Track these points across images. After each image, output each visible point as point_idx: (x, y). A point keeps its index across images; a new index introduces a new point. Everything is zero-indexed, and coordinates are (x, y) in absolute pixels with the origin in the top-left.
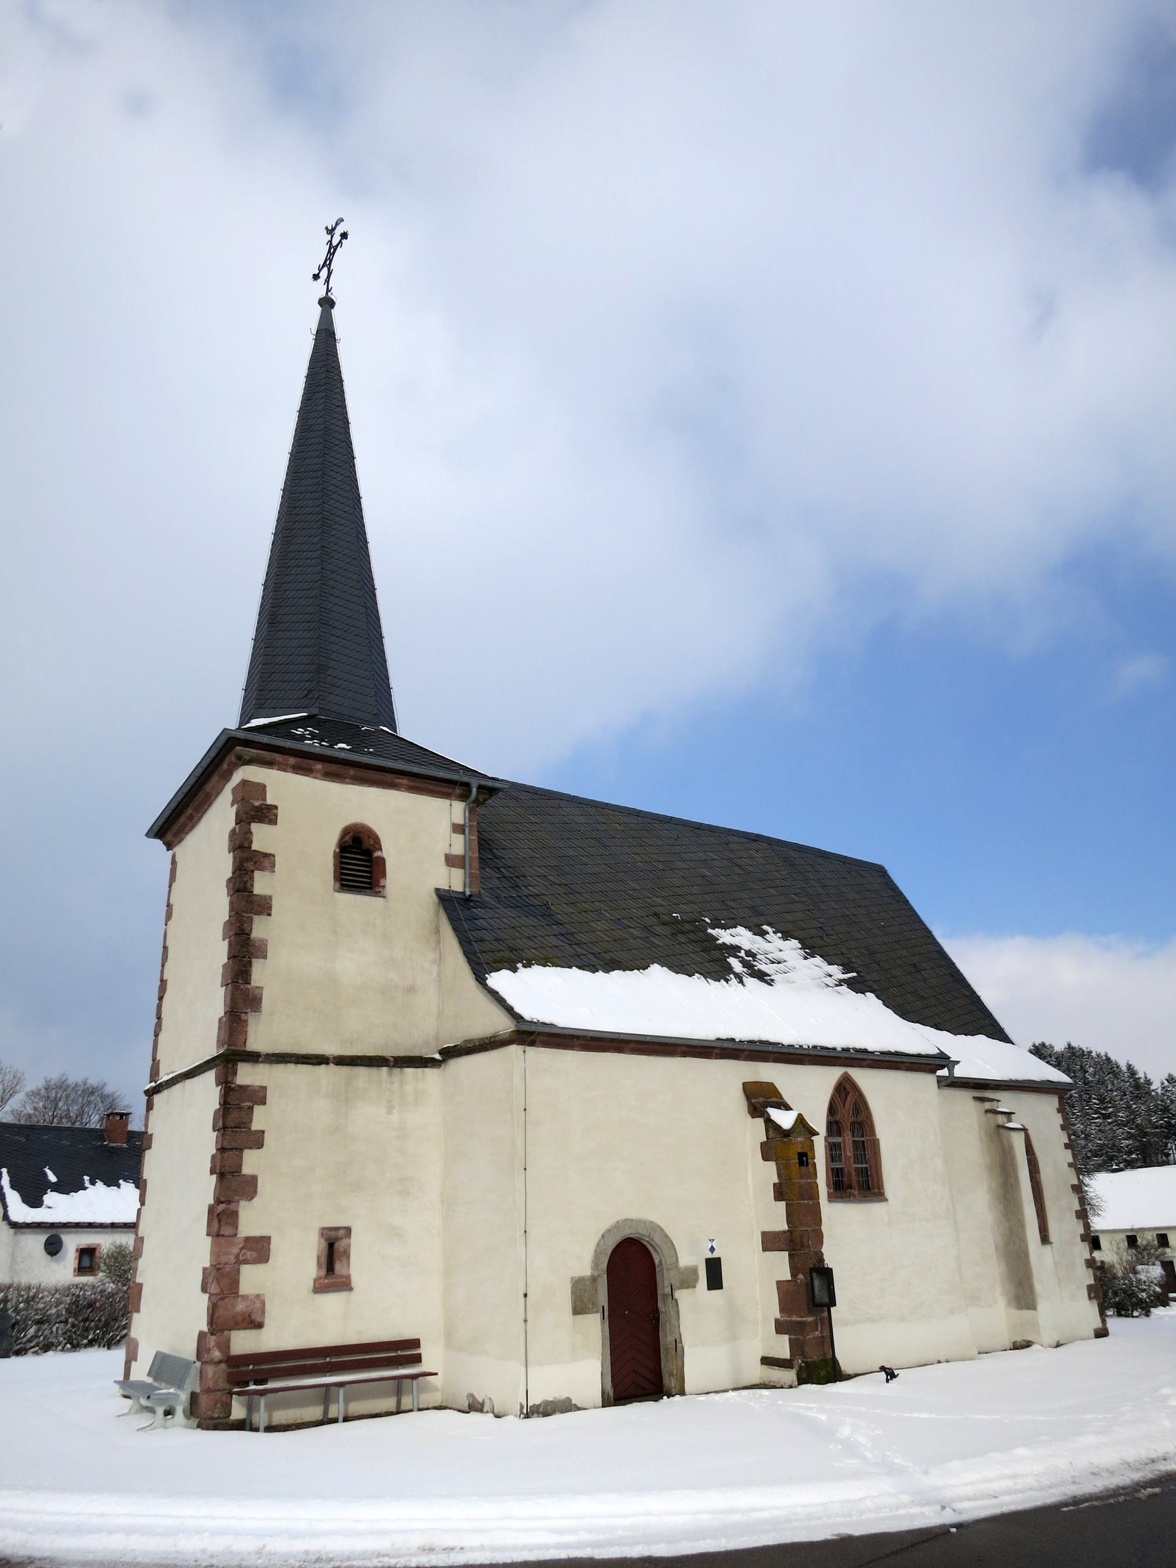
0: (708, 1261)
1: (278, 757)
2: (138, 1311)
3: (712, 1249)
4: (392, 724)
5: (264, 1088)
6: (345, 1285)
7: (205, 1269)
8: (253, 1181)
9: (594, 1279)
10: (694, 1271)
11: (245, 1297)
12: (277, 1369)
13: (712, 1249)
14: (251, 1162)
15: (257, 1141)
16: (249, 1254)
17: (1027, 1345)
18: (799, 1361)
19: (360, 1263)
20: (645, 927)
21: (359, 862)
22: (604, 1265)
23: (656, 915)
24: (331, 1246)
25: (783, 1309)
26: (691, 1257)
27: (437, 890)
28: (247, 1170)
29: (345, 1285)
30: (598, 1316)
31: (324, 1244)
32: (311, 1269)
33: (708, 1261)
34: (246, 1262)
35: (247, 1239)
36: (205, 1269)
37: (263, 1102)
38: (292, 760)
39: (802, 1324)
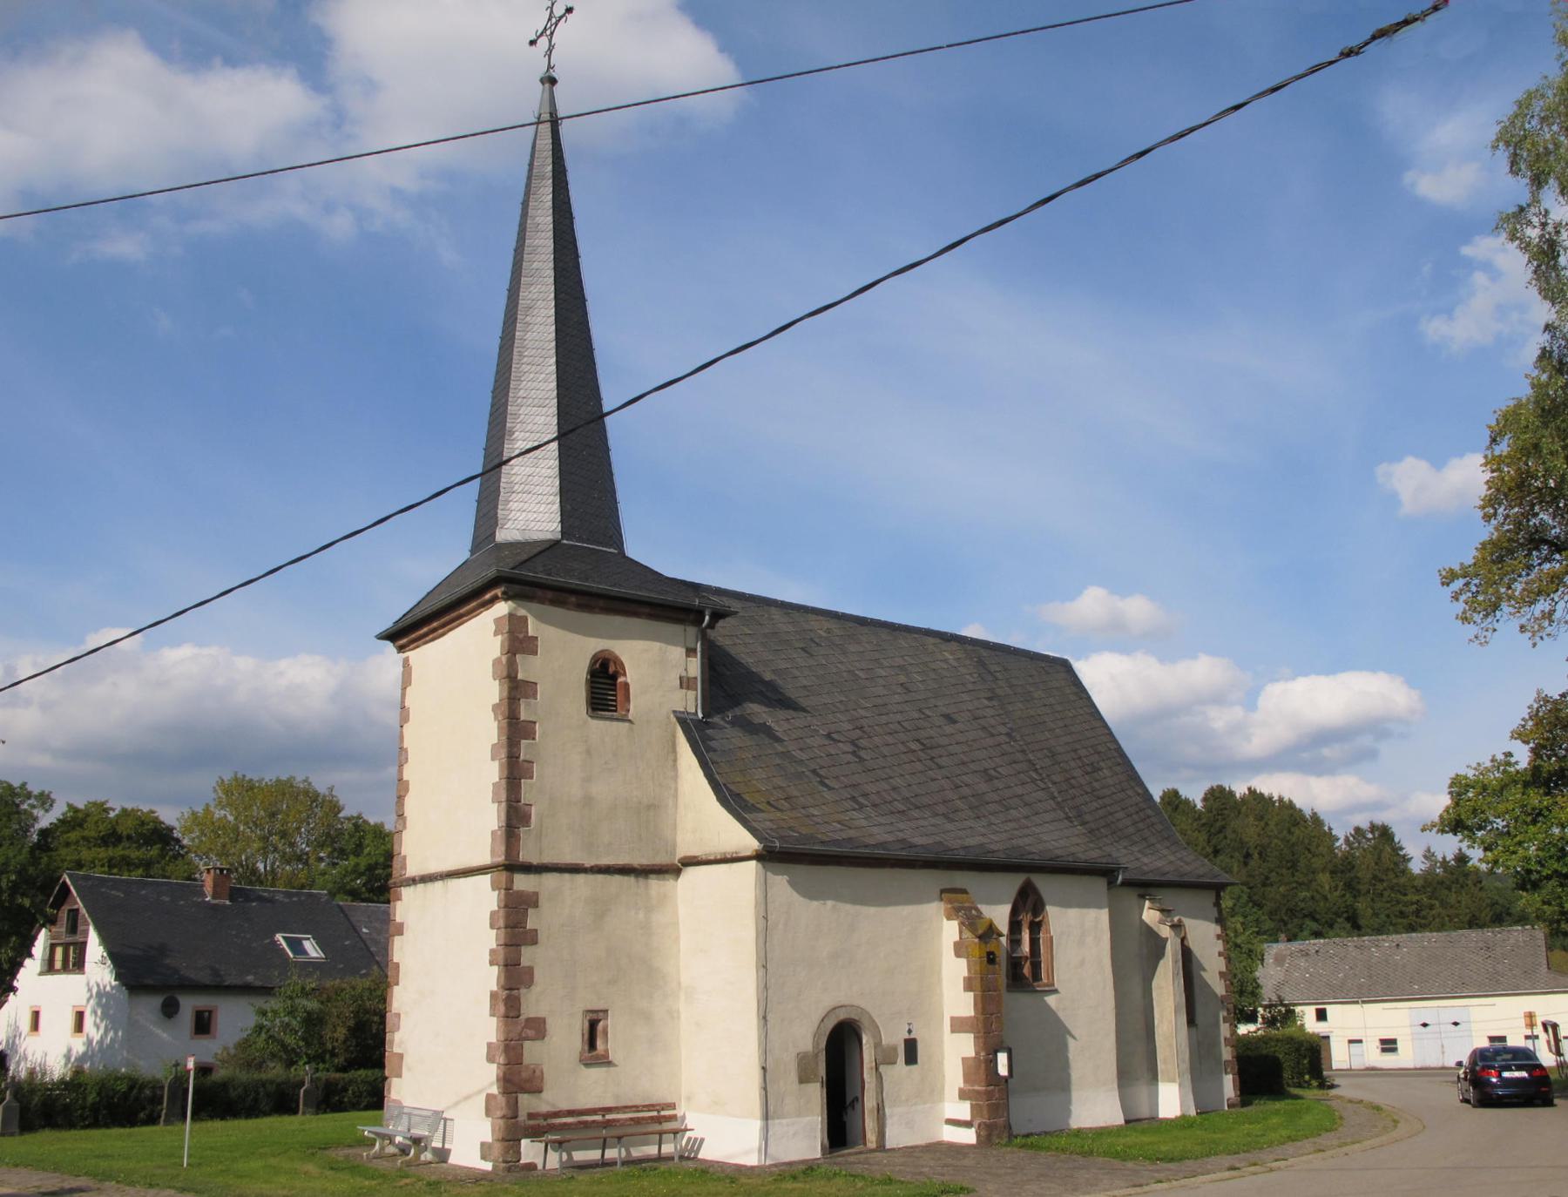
0: (907, 1041)
1: (539, 593)
2: (399, 1076)
3: (910, 1031)
4: (618, 542)
5: (536, 894)
6: (605, 1061)
7: (489, 1045)
8: (530, 971)
9: (816, 1055)
10: (894, 1049)
11: (527, 1067)
12: (585, 1123)
13: (910, 1031)
14: (528, 955)
15: (532, 938)
16: (530, 1033)
17: (1351, 1042)
18: (976, 1123)
19: (615, 1041)
20: (853, 743)
21: (604, 687)
22: (823, 1045)
23: (861, 728)
24: (593, 1025)
25: (967, 1079)
26: (894, 1037)
27: (674, 712)
28: (525, 962)
29: (605, 1061)
30: (818, 1085)
31: (587, 1024)
32: (577, 1042)
33: (907, 1041)
34: (527, 1039)
35: (528, 1020)
36: (489, 1045)
37: (536, 905)
38: (550, 594)
39: (251, 883)
